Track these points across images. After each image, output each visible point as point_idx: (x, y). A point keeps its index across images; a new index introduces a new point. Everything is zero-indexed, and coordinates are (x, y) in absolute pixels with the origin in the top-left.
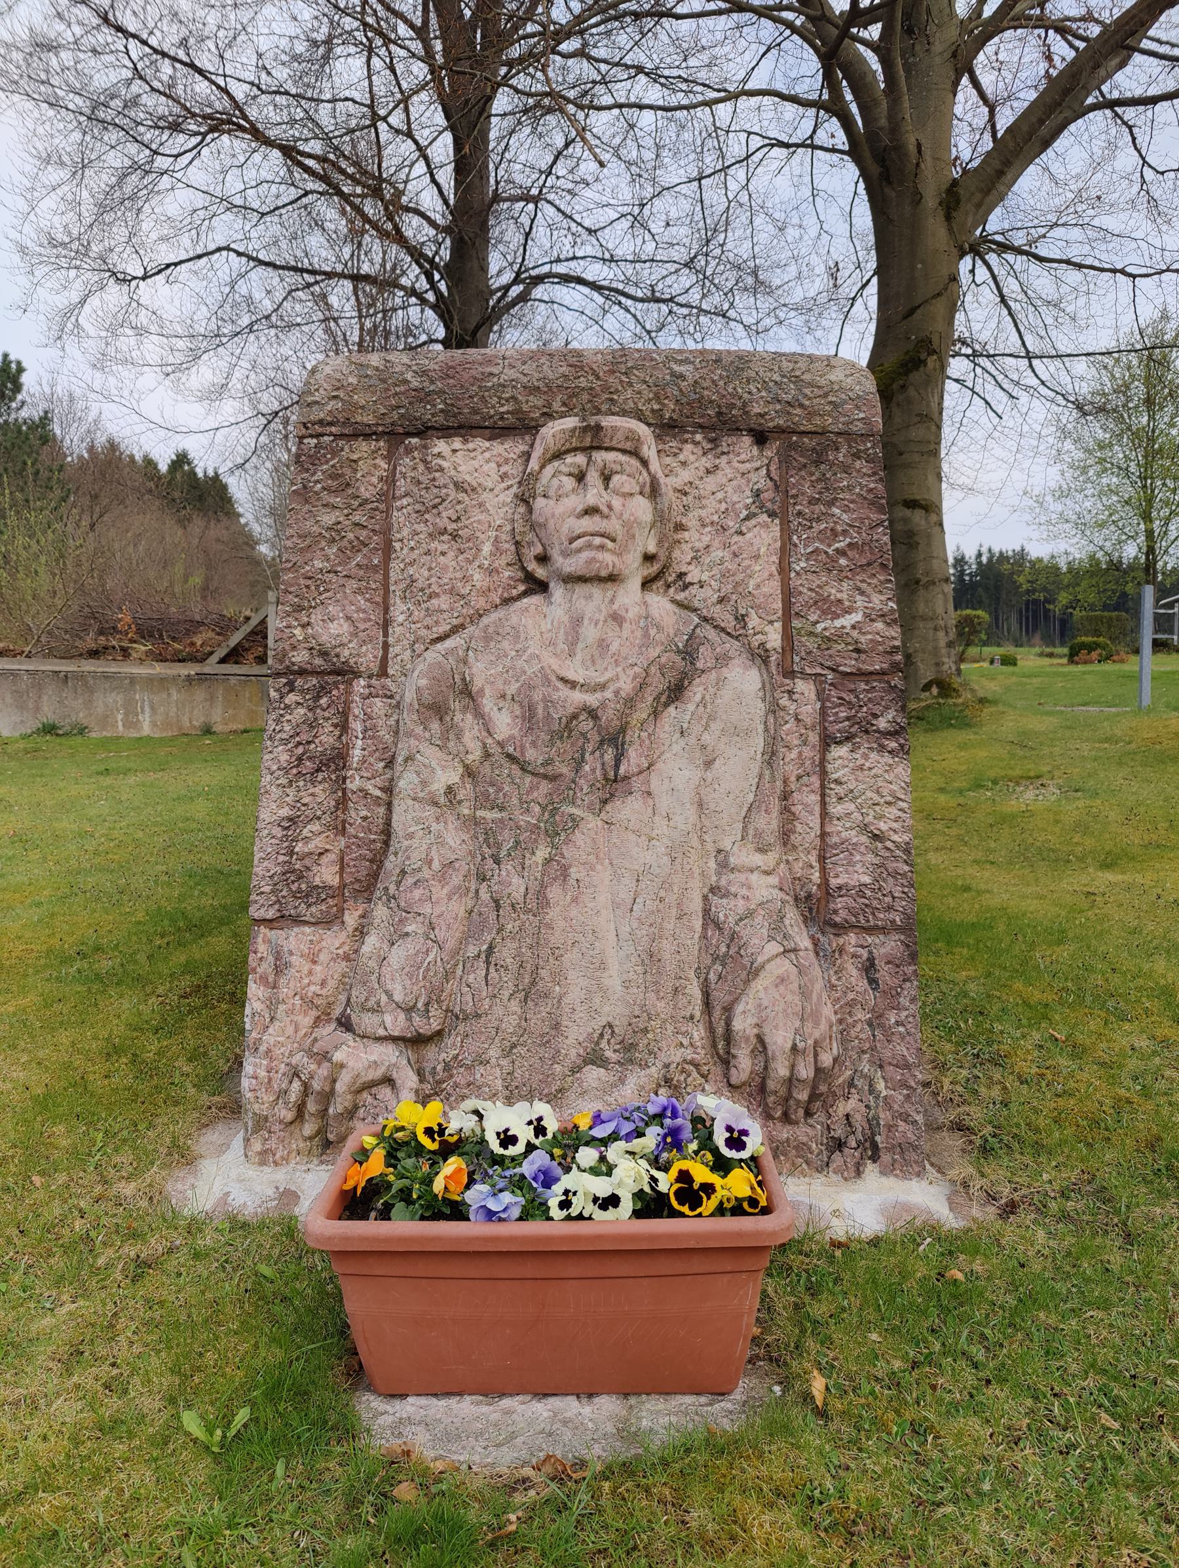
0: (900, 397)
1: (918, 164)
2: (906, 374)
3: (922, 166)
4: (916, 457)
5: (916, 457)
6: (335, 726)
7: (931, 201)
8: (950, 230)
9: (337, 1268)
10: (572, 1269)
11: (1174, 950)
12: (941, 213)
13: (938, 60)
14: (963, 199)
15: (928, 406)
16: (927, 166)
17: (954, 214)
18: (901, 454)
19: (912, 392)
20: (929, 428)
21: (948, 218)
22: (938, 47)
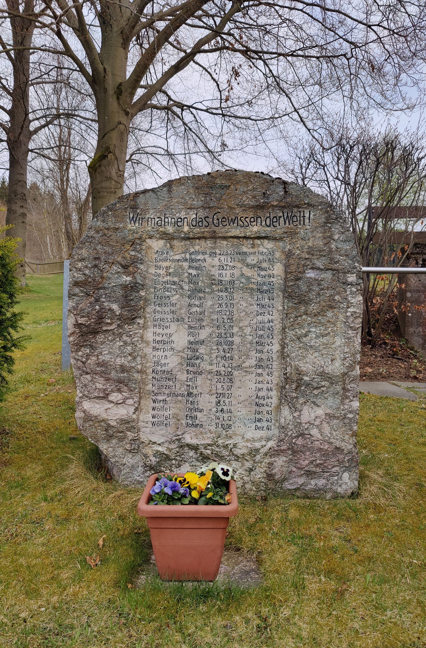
0: (99, 170)
1: (104, 77)
2: (101, 161)
3: (107, 77)
4: (105, 194)
5: (105, 194)
6: (273, 210)
7: (111, 91)
8: (119, 103)
9: (151, 525)
10: (165, 524)
11: (425, 388)
12: (115, 97)
13: (115, 34)
14: (123, 91)
15: (110, 173)
16: (109, 77)
17: (120, 97)
18: (99, 193)
19: (103, 168)
20: (111, 182)
21: (118, 99)
22: (115, 29)
